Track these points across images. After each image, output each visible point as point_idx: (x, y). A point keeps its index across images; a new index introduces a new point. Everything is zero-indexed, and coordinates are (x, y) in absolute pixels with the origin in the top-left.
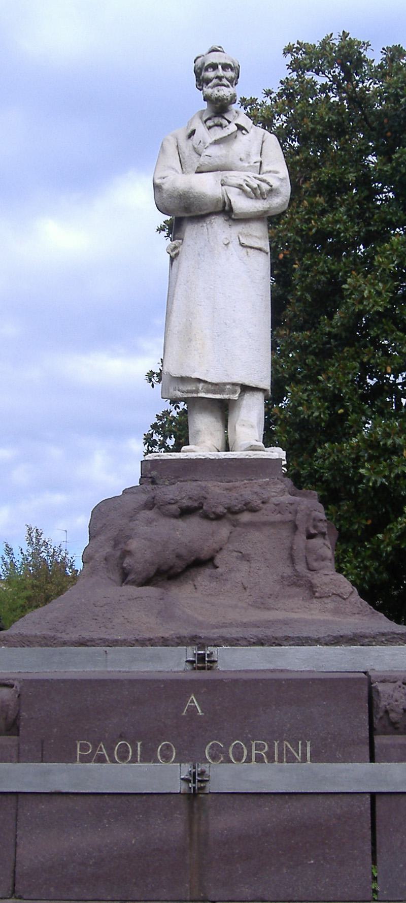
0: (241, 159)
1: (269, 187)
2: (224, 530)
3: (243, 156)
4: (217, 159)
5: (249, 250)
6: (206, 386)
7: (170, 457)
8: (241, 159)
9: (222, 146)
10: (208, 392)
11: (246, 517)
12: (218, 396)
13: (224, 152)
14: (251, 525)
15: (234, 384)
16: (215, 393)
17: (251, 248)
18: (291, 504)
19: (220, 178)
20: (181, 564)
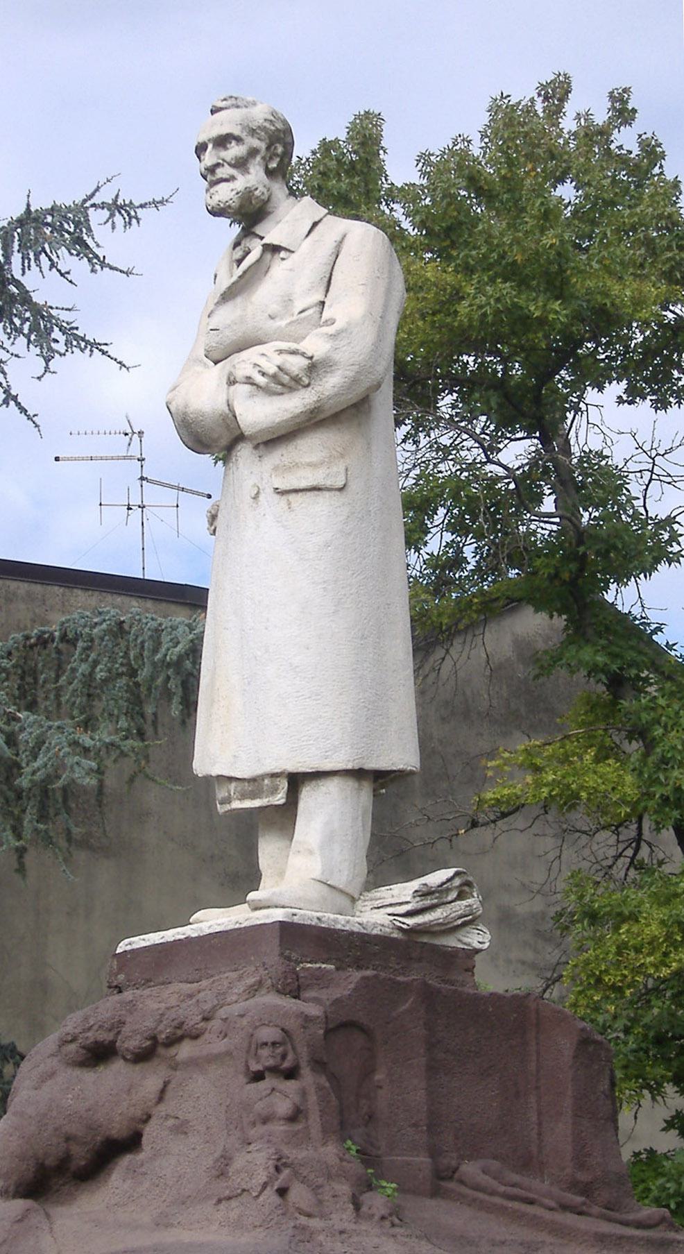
0: (271, 317)
1: (307, 362)
2: (150, 1080)
3: (274, 308)
4: (227, 332)
5: (292, 497)
6: (240, 786)
7: (148, 944)
8: (271, 317)
9: (239, 300)
10: (243, 797)
11: (185, 1050)
12: (257, 803)
13: (239, 312)
14: (194, 1063)
15: (274, 775)
16: (253, 796)
17: (296, 491)
18: (242, 1016)
19: (226, 372)
20: (81, 1156)
